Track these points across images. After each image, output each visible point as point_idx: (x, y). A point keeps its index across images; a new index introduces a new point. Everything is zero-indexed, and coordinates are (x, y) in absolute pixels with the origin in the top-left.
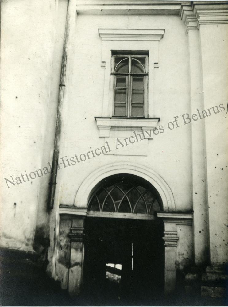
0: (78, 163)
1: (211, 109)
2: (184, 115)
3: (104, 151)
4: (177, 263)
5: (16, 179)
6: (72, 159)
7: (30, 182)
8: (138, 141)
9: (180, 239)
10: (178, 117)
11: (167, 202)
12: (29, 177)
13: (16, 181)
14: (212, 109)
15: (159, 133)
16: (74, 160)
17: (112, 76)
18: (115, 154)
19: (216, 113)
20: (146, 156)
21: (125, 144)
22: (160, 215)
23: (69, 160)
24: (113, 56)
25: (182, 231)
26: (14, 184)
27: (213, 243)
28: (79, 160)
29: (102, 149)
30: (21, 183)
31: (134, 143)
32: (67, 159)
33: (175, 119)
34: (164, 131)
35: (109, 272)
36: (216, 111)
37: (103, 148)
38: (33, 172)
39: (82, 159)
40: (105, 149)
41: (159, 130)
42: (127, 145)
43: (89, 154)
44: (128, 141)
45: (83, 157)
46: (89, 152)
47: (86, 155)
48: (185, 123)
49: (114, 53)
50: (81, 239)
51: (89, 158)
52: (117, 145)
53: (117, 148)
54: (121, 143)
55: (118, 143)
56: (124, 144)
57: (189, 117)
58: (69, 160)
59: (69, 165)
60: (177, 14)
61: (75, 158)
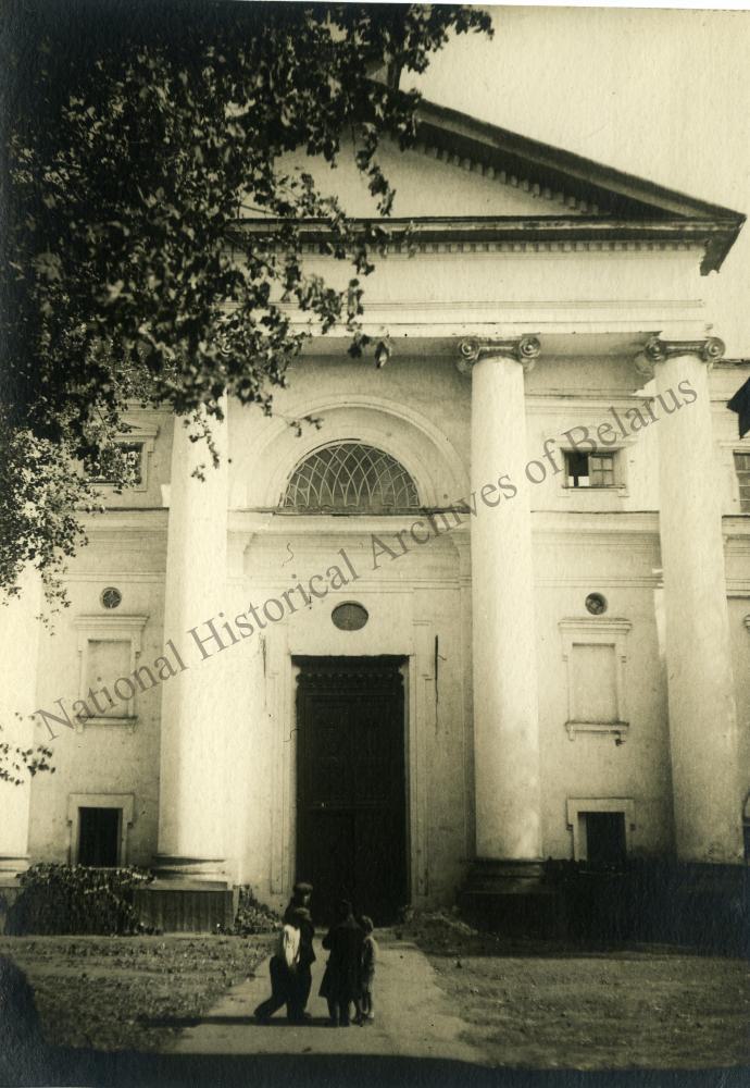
6: (242, 620)
12: (285, 604)
13: (630, 420)
15: (503, 498)
19: (670, 412)
20: (437, 639)
26: (69, 724)
28: (263, 619)
29: (328, 574)
32: (224, 623)
35: (413, 18)
36: (671, 405)
38: (274, 601)
39: (533, 475)
40: (339, 572)
41: (500, 492)
43: (291, 596)
45: (274, 611)
46: (292, 591)
53: (376, 567)
58: (230, 625)
59: (235, 641)
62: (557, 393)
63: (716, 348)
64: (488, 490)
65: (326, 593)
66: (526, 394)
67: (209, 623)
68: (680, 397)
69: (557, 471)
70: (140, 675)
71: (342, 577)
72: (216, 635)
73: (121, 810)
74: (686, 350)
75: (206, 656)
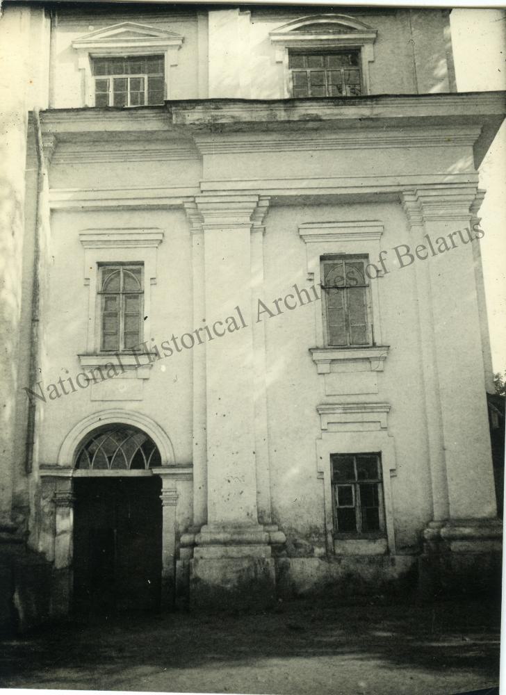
0: (230, 333)
2: (399, 249)
7: (207, 323)
8: (302, 304)
10: (385, 252)
11: (166, 455)
13: (49, 392)
14: (458, 233)
16: (169, 346)
17: (99, 296)
18: (104, 399)
19: (465, 243)
21: (275, 311)
22: (156, 471)
24: (100, 268)
25: (181, 486)
27: (211, 500)
28: (180, 346)
33: (380, 257)
37: (230, 321)
40: (234, 321)
42: (280, 312)
43: (200, 333)
44: (281, 304)
45: (187, 340)
47: (195, 336)
48: (402, 266)
49: (100, 264)
50: (67, 503)
51: (201, 342)
52: (259, 313)
54: (267, 310)
55: (262, 309)
57: (410, 253)
60: (179, 208)
61: (172, 343)
62: (449, 203)
69: (317, 298)
70: (468, 238)
71: (446, 245)
73: (379, 455)
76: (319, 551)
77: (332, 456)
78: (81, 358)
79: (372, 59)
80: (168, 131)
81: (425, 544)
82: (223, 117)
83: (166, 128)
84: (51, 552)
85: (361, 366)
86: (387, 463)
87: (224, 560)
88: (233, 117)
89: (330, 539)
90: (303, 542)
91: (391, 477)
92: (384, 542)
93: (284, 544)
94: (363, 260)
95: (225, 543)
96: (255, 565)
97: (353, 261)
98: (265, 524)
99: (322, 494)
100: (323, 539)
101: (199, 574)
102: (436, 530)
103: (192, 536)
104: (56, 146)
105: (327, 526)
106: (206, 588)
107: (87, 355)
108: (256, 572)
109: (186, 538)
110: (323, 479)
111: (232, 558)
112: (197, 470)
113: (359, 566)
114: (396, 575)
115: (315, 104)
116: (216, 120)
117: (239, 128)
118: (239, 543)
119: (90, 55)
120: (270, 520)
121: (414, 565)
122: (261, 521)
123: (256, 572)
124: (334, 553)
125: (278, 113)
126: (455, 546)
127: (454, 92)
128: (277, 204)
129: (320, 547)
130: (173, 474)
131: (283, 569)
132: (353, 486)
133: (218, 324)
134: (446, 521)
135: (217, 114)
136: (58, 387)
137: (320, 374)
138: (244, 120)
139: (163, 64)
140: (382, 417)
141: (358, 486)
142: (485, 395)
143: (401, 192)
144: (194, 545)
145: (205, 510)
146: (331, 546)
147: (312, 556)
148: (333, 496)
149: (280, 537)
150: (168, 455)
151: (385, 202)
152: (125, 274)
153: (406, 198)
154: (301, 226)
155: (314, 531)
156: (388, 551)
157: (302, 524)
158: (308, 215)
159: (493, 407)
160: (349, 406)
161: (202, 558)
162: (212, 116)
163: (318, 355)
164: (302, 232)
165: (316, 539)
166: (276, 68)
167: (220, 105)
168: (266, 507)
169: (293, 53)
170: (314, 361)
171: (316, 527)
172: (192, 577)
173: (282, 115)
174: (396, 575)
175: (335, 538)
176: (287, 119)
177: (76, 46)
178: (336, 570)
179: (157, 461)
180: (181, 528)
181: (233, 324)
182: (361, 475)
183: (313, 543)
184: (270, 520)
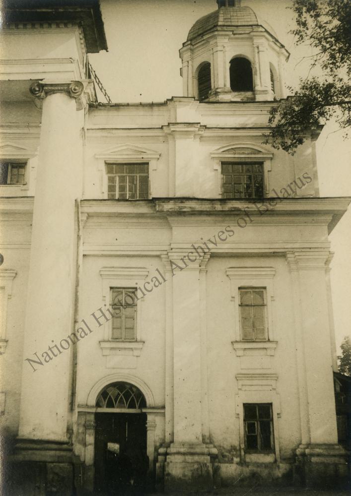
1: (291, 183)
3: (157, 284)
4: (155, 442)
5: (43, 356)
9: (157, 426)
11: (149, 401)
13: (44, 358)
14: (293, 183)
22: (144, 410)
23: (302, 178)
26: (41, 363)
29: (152, 281)
30: (51, 359)
31: (152, 291)
34: (234, 233)
37: (283, 191)
40: (157, 280)
44: (186, 260)
49: (111, 288)
56: (183, 265)
63: (77, 88)
64: (221, 233)
65: (196, 260)
66: (32, 213)
67: (100, 310)
68: (304, 180)
72: (104, 315)
73: (271, 404)
74: (58, 90)
75: (100, 325)
76: (236, 460)
77: (244, 404)
78: (101, 343)
79: (270, 170)
80: (153, 213)
81: (297, 458)
82: (185, 207)
83: (152, 212)
84: (83, 454)
85: (263, 352)
86: (275, 410)
87: (184, 463)
88: (190, 208)
89: (243, 453)
90: (227, 454)
91: (278, 418)
92: (273, 455)
93: (217, 455)
94: (263, 290)
95: (184, 454)
96: (201, 467)
97: (257, 290)
98: (207, 443)
99: (238, 427)
100: (238, 453)
101: (170, 472)
102: (303, 450)
103: (165, 449)
104: (87, 218)
105: (241, 445)
106: (173, 479)
107: (104, 341)
108: (201, 471)
109: (161, 450)
110: (239, 418)
111: (188, 463)
112: (168, 409)
113: (259, 470)
114: (280, 475)
115: (238, 202)
116: (181, 209)
117: (193, 213)
118: (192, 454)
119: (105, 161)
120: (208, 441)
121: (291, 470)
122: (204, 442)
123: (201, 471)
124: (245, 461)
125: (216, 206)
126: (314, 459)
127: (318, 197)
128: (214, 256)
129: (237, 458)
130: (155, 413)
131: (216, 470)
132: (256, 422)
133: (147, 284)
134: (309, 445)
135: (182, 205)
136: (50, 353)
137: (237, 356)
138: (197, 210)
139: (148, 169)
140: (273, 383)
141: (259, 422)
142: (332, 372)
143: (286, 252)
144: (166, 454)
145: (172, 434)
146: (243, 457)
147: (232, 463)
148: (245, 429)
149: (215, 451)
150: (150, 399)
151: (278, 256)
152: (126, 294)
153: (288, 256)
154: (227, 270)
155: (233, 448)
156: (276, 461)
157: (227, 445)
158: (234, 263)
159: (337, 380)
160: (254, 376)
161: (171, 462)
162: (179, 207)
163: (237, 346)
164: (228, 273)
165: (235, 453)
166: (213, 173)
167: (184, 201)
168: (207, 434)
169: (223, 163)
170: (234, 349)
171: (234, 446)
172: (165, 473)
173: (218, 207)
174: (280, 475)
175: (245, 453)
176: (221, 209)
177: (96, 157)
178: (247, 471)
179: (143, 404)
180: (158, 444)
181: (157, 281)
182: (260, 415)
183: (233, 455)
184: (208, 441)
